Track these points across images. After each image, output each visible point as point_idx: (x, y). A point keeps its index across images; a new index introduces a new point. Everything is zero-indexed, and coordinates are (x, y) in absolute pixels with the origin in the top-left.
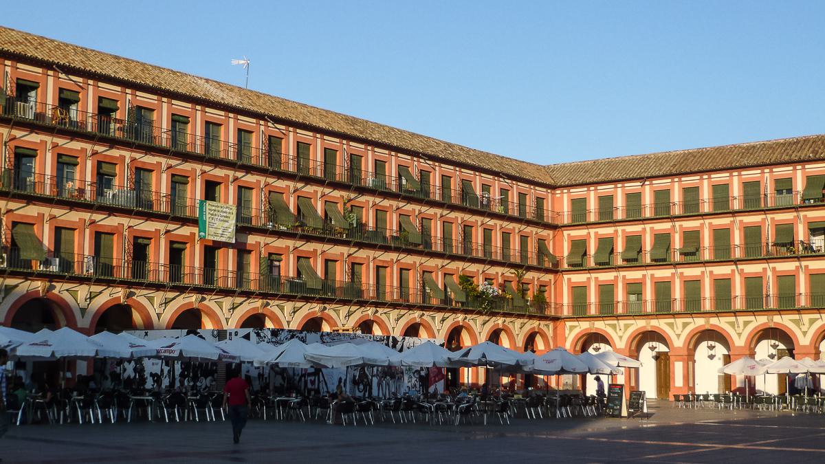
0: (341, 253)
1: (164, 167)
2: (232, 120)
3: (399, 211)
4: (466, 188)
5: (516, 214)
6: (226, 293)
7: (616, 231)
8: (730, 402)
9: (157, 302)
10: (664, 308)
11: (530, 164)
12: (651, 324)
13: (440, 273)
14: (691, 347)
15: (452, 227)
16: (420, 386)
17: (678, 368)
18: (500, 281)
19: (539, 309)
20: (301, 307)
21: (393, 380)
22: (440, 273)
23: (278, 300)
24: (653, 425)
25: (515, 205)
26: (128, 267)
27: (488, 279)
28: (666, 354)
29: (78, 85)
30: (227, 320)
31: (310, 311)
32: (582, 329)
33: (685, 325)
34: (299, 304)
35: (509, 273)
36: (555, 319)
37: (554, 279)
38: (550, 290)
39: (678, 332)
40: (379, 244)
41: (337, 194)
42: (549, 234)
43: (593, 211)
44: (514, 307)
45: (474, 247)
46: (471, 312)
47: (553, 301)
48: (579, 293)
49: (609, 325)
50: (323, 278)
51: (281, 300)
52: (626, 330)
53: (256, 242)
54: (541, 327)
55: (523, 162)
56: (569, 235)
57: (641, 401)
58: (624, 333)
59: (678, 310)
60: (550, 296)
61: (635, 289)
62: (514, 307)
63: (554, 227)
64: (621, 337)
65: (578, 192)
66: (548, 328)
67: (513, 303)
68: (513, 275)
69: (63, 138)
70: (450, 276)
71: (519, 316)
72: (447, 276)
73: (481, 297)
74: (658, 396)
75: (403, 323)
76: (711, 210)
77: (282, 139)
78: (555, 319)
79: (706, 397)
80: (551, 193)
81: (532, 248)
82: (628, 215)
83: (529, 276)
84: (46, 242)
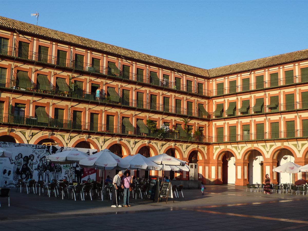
0: (205, 124)
1: (161, 94)
2: (161, 70)
3: (107, 85)
4: (153, 76)
5: (185, 90)
6: (102, 134)
7: (238, 99)
8: (303, 190)
9: (27, 135)
10: (260, 138)
11: (199, 68)
12: (254, 146)
13: (134, 118)
15: (192, 104)
16: (75, 176)
18: (173, 124)
19: (199, 138)
20: (109, 139)
21: (52, 173)
22: (134, 118)
23: (155, 140)
24: (290, 201)
25: (184, 86)
26: (120, 129)
27: (166, 123)
30: (160, 150)
31: (43, 135)
32: (221, 149)
33: (271, 146)
34: (189, 145)
35: (179, 120)
36: (208, 144)
37: (208, 124)
38: (206, 129)
39: (268, 150)
40: (90, 101)
41: (65, 74)
42: (205, 102)
43: (226, 89)
44: (180, 137)
45: (182, 110)
46: (153, 139)
47: (207, 135)
48: (220, 130)
49: (234, 147)
50: (53, 118)
51: (128, 138)
52: (242, 149)
53: (6, 97)
54: (200, 148)
55: (195, 67)
56: (215, 102)
57: (168, 190)
58: (241, 151)
60: (206, 133)
61: (246, 128)
62: (180, 137)
63: (208, 98)
64: (239, 153)
65: (220, 80)
66: (204, 149)
67: (179, 135)
68: (182, 121)
69: (59, 70)
70: (141, 120)
72: (139, 120)
73: (157, 131)
75: (108, 143)
77: (181, 78)
78: (208, 144)
79: (285, 185)
80: (207, 81)
81: (194, 108)
82: (218, 94)
83: (192, 122)
84: (134, 125)
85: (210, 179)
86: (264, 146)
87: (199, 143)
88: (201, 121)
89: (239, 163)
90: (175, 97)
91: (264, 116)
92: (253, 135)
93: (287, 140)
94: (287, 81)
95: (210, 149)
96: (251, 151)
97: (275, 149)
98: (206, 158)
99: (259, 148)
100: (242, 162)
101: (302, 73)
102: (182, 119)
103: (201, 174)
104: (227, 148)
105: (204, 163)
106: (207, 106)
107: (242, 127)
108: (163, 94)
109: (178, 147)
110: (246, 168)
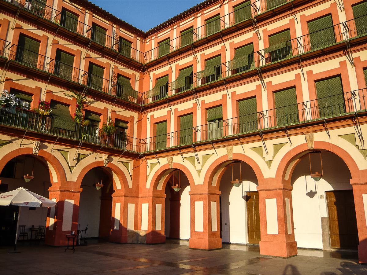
10: (251, 131)
12: (234, 152)
14: (287, 178)
17: (271, 207)
28: (256, 193)
29: (80, 11)
32: (162, 165)
33: (277, 148)
35: (59, 92)
36: (136, 156)
38: (132, 127)
47: (135, 135)
52: (204, 162)
59: (266, 127)
64: (199, 171)
68: (71, 99)
71: (73, 144)
74: (249, 241)
76: (273, 126)
78: (136, 156)
83: (99, 105)
85: (138, 231)
86: (258, 150)
87: (112, 152)
88: (122, 108)
89: (198, 194)
90: (55, 43)
91: (256, 80)
92: (230, 127)
93: (322, 124)
94: (241, 126)
95: (141, 167)
96: (227, 166)
97: (289, 152)
98: (130, 185)
99: (245, 154)
100: (204, 192)
101: (309, 29)
102: (70, 93)
103: (119, 219)
104: (174, 162)
105: (125, 196)
106: (137, 84)
107: (206, 114)
108: (18, 27)
109: (53, 154)
110: (214, 205)
